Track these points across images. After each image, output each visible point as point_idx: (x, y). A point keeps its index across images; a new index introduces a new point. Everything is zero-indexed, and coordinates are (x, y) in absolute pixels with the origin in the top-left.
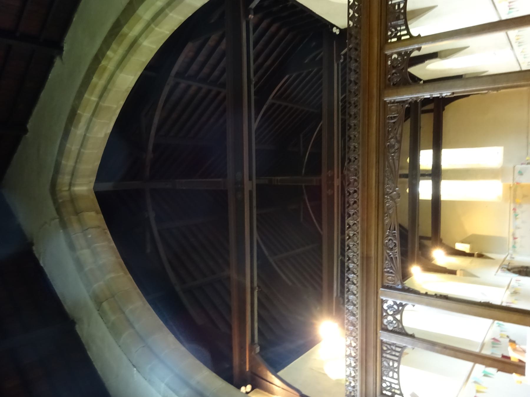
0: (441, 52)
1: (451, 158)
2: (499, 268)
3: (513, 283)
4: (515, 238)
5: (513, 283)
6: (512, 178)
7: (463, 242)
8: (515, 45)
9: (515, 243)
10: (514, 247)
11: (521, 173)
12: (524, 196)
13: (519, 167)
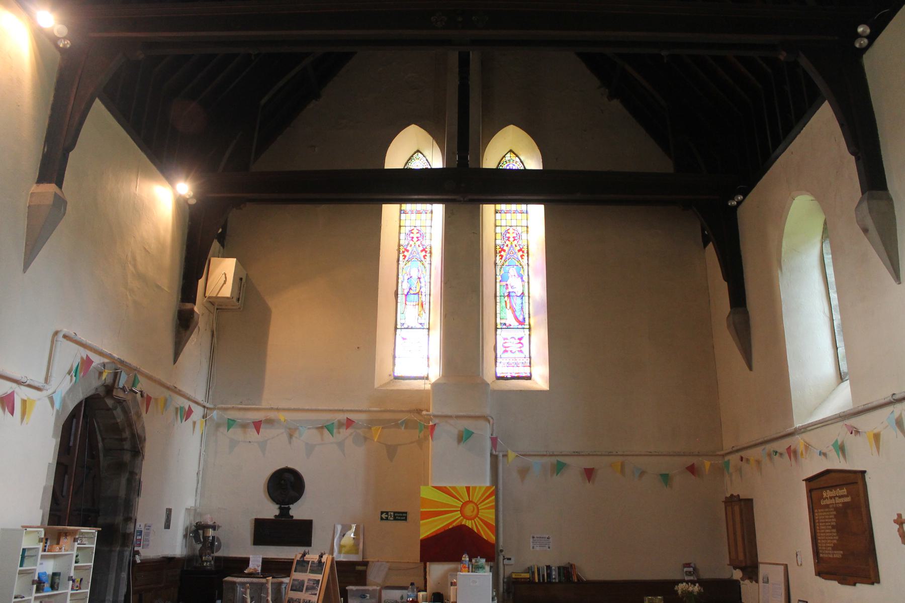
0: (890, 200)
1: (518, 229)
4: (257, 425)
6: (447, 411)
7: (242, 282)
9: (244, 426)
10: (231, 423)
12: (392, 451)
13: (485, 431)
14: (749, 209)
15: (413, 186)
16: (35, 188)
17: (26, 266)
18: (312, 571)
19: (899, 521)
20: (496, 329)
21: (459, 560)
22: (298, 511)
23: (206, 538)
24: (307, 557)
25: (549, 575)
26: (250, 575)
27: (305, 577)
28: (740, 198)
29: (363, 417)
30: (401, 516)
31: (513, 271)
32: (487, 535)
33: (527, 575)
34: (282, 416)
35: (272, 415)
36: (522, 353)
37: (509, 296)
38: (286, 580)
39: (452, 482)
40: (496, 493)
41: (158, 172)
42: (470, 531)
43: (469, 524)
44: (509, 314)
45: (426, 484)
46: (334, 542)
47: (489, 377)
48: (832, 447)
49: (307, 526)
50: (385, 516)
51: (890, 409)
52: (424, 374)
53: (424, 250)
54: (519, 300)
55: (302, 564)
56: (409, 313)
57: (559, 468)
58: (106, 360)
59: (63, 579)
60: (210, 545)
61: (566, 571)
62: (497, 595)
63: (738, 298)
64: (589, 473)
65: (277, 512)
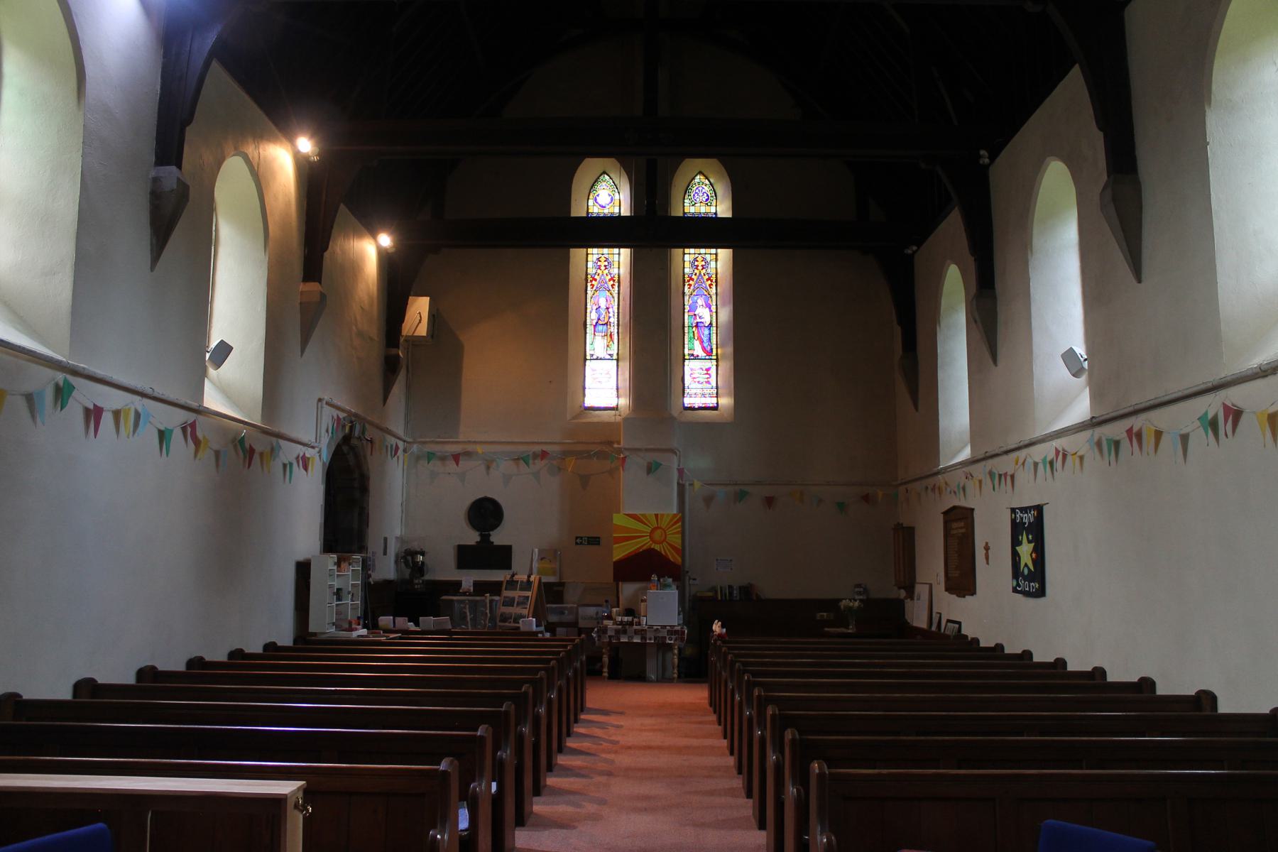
0: (994, 298)
1: (706, 274)
2: (349, 412)
4: (456, 458)
5: (290, 452)
6: (638, 445)
7: (434, 317)
9: (443, 459)
10: (430, 456)
11: (651, 469)
12: (585, 480)
14: (1000, 173)
15: (605, 231)
16: (304, 287)
17: (303, 351)
18: (522, 589)
20: (684, 359)
21: (647, 578)
22: (498, 538)
23: (415, 563)
24: (516, 578)
25: (731, 594)
26: (464, 594)
27: (516, 594)
28: (915, 248)
29: (557, 448)
30: (594, 541)
31: (701, 301)
32: (674, 557)
33: (710, 594)
34: (479, 449)
35: (469, 448)
36: (703, 383)
37: (697, 326)
38: (497, 598)
39: (642, 507)
40: (682, 519)
41: (276, 131)
42: (658, 553)
43: (657, 547)
44: (697, 343)
45: (618, 511)
46: (528, 566)
47: (675, 412)
48: (1198, 423)
49: (507, 550)
50: (579, 541)
51: (983, 463)
52: (613, 404)
53: (612, 279)
54: (706, 332)
55: (512, 584)
56: (597, 344)
57: (741, 496)
58: (342, 415)
59: (344, 594)
60: (419, 569)
61: (747, 591)
62: (683, 610)
63: (910, 343)
64: (770, 501)
65: (478, 539)
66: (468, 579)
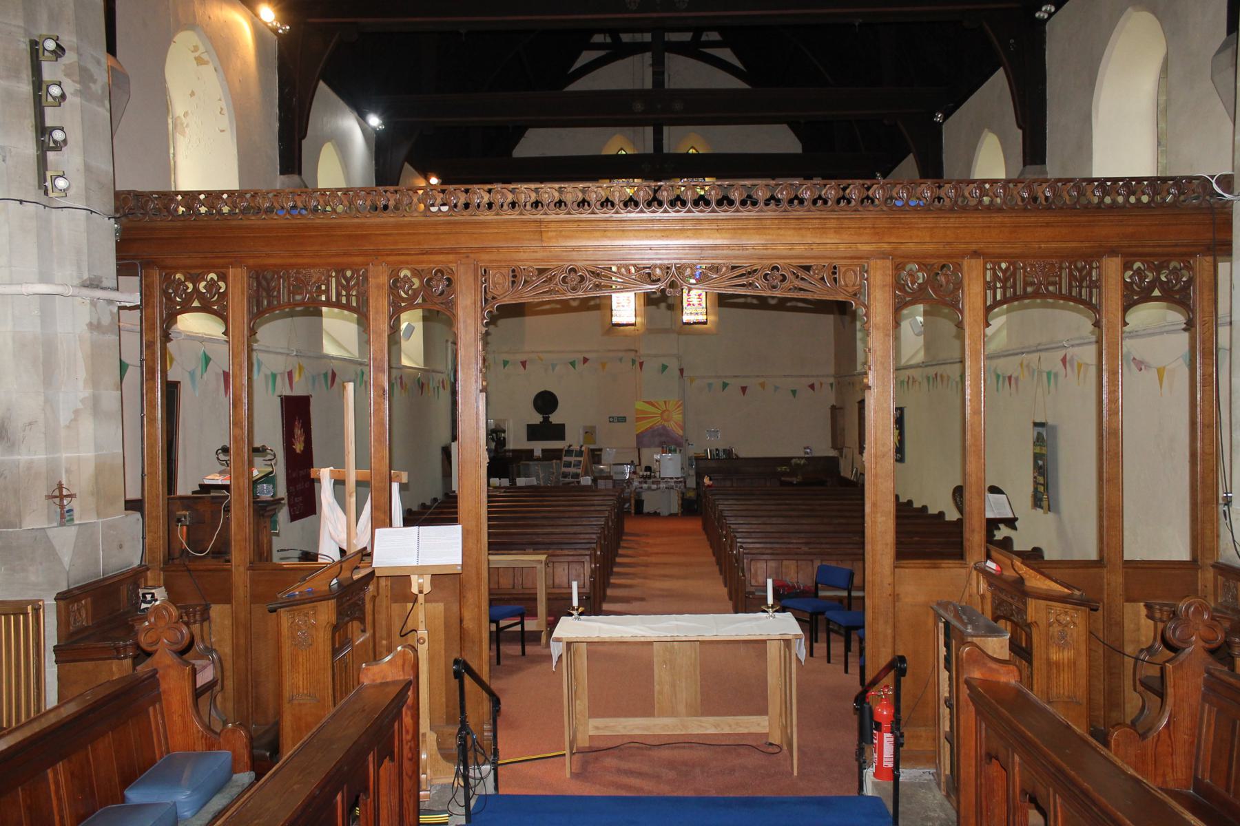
3: (440, 377)
8: (931, 371)
19: (446, 823)
22: (555, 418)
27: (573, 459)
50: (612, 420)
66: (538, 447)
